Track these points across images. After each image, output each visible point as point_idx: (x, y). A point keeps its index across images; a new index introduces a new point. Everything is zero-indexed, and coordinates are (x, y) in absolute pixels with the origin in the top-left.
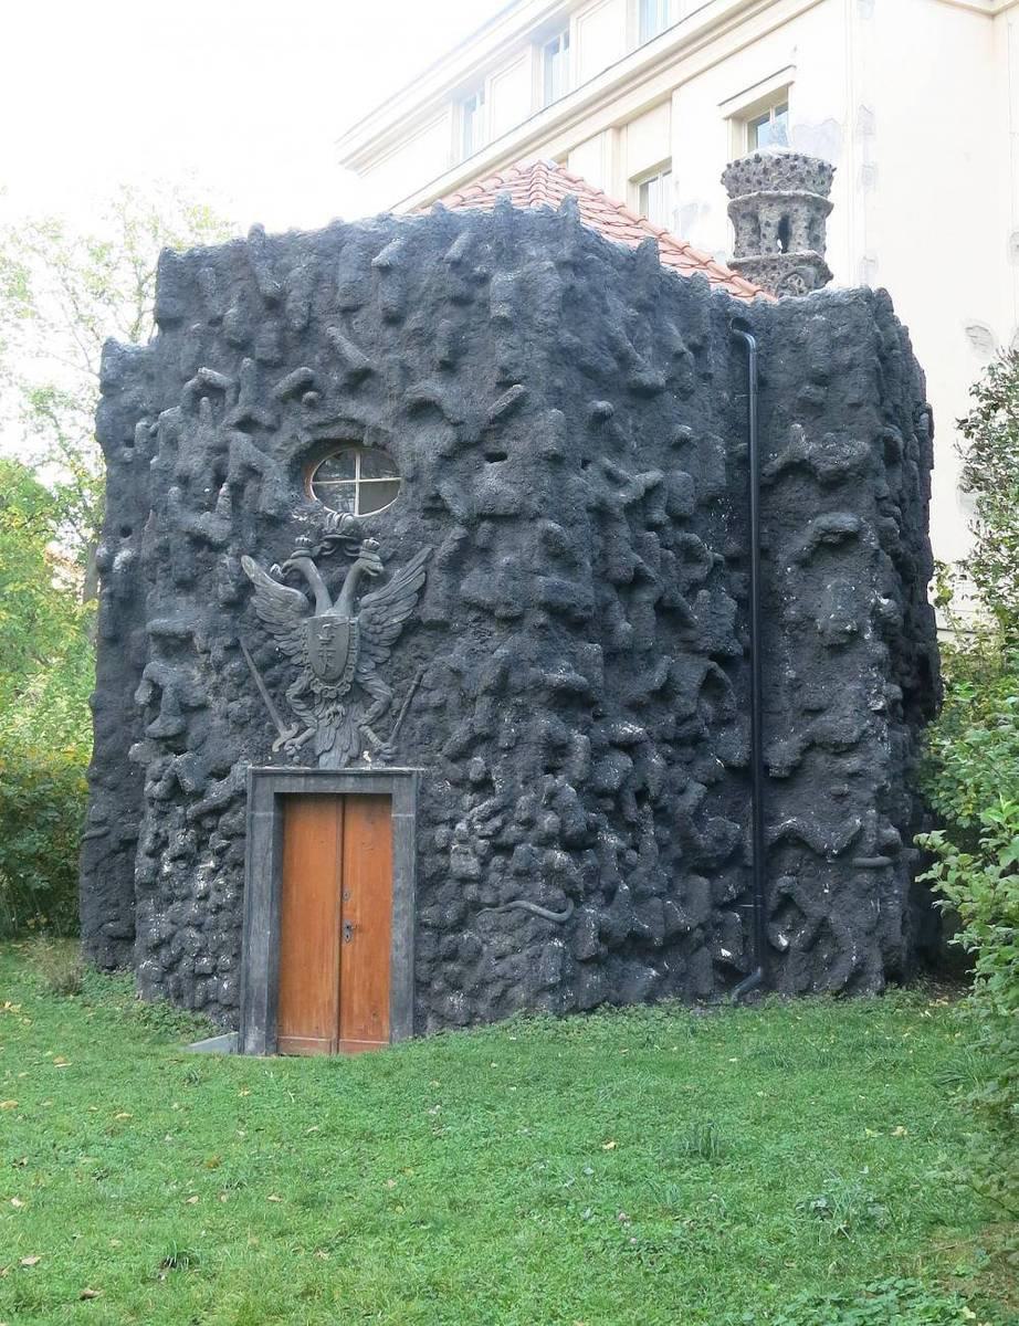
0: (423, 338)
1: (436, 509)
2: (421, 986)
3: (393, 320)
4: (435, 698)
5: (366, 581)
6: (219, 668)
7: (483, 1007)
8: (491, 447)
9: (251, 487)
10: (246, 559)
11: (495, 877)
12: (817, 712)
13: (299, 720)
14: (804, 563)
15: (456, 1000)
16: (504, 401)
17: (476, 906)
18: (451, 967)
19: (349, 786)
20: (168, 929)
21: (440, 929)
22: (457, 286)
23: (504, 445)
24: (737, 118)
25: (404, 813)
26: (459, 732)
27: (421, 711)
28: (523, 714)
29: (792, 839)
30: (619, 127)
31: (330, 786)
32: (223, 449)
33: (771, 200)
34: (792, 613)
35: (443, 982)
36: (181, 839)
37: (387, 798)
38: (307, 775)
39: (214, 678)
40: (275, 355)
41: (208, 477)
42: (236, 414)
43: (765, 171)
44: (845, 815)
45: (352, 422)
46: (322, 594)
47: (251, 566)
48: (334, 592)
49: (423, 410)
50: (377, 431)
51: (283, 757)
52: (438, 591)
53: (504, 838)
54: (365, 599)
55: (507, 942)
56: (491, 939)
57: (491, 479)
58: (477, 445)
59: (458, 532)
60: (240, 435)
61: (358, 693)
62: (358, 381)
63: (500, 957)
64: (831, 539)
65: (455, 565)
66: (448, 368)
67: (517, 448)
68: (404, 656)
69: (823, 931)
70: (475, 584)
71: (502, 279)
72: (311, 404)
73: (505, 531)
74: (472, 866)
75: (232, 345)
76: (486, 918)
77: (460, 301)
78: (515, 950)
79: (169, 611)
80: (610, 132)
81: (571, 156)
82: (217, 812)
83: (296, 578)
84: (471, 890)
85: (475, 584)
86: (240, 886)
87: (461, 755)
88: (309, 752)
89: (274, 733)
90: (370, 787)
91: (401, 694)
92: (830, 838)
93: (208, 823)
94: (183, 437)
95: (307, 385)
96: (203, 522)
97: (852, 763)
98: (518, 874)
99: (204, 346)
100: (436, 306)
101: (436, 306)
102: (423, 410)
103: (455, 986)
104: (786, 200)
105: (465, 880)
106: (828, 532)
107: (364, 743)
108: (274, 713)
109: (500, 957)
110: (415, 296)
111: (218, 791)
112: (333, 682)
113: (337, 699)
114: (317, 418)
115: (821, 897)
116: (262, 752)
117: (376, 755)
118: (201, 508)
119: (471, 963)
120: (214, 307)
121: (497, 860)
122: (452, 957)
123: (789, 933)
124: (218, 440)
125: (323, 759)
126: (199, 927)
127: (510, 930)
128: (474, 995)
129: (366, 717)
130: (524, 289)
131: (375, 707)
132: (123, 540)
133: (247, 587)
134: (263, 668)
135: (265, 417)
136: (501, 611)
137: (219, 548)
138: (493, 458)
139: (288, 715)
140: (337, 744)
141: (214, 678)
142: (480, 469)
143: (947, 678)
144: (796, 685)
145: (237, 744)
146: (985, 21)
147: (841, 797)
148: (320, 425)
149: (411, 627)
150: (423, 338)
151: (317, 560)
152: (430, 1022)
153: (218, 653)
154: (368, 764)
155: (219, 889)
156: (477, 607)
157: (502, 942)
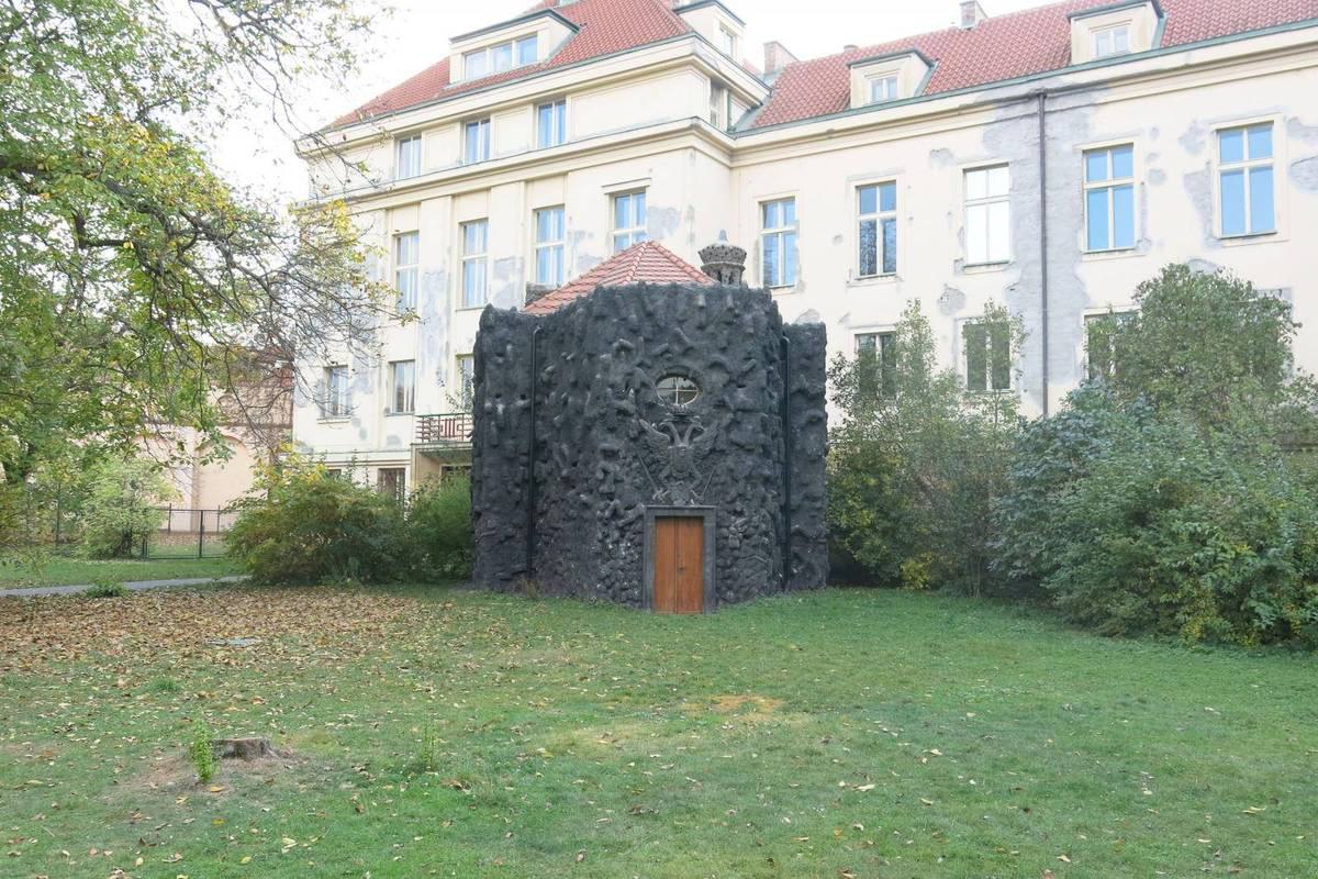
0: (713, 336)
1: (721, 405)
2: (718, 589)
3: (701, 327)
4: (723, 479)
5: (696, 432)
6: (630, 465)
7: (741, 596)
8: (740, 382)
9: (643, 390)
10: (641, 421)
11: (744, 547)
12: (806, 485)
13: (663, 486)
14: (802, 429)
15: (730, 594)
16: (746, 367)
17: (737, 558)
18: (729, 582)
19: (687, 513)
20: (609, 572)
21: (725, 567)
22: (729, 318)
23: (745, 382)
24: (611, 195)
25: (710, 524)
26: (733, 493)
27: (716, 485)
28: (754, 486)
29: (799, 533)
30: (403, 138)
31: (678, 513)
32: (631, 374)
33: (728, 266)
34: (798, 447)
35: (725, 589)
36: (616, 534)
37: (701, 519)
38: (669, 509)
39: (627, 469)
40: (651, 337)
41: (624, 386)
42: (638, 360)
43: (726, 253)
44: (815, 524)
45: (684, 367)
46: (677, 437)
47: (645, 424)
48: (682, 435)
49: (716, 365)
50: (695, 372)
51: (657, 501)
52: (723, 438)
53: (748, 532)
54: (695, 440)
55: (750, 571)
56: (744, 571)
57: (741, 395)
58: (736, 382)
59: (730, 416)
60: (638, 369)
61: (691, 477)
62: (687, 351)
63: (747, 577)
64: (814, 420)
65: (728, 429)
66: (723, 350)
67: (750, 383)
68: (708, 463)
69: (810, 567)
70: (735, 436)
71: (748, 317)
72: (669, 360)
73: (746, 415)
74: (737, 543)
75: (631, 330)
76: (741, 562)
77: (729, 324)
78: (752, 574)
79: (605, 440)
80: (523, 183)
81: (493, 190)
82: (631, 524)
83: (665, 429)
84: (736, 553)
85: (735, 436)
86: (641, 553)
87: (733, 501)
88: (669, 499)
89: (653, 492)
90: (696, 514)
91: (706, 477)
92: (811, 532)
93: (627, 528)
94: (612, 367)
95: (667, 351)
96: (624, 404)
97: (818, 505)
98: (754, 546)
99: (619, 328)
100: (718, 324)
101: (718, 324)
102: (716, 365)
103: (730, 588)
104: (733, 267)
105: (733, 549)
106: (814, 417)
107: (692, 496)
108: (653, 483)
109: (747, 577)
110: (711, 319)
111: (631, 514)
112: (681, 472)
113: (683, 479)
114: (671, 365)
115: (809, 555)
116: (647, 500)
117: (696, 501)
118: (622, 399)
119: (735, 580)
120: (623, 312)
121: (746, 541)
122: (729, 577)
123: (796, 568)
124: (630, 371)
125: (675, 503)
126: (622, 570)
127: (751, 567)
128: (736, 592)
129: (692, 486)
130: (755, 320)
131: (696, 482)
132: (498, 400)
133: (643, 432)
134: (649, 466)
135: (648, 362)
136: (748, 447)
137: (631, 415)
138: (740, 387)
139: (659, 484)
140: (681, 497)
141: (627, 469)
142: (735, 391)
143: (796, 470)
144: (798, 475)
145: (637, 496)
146: (726, 171)
147: (813, 517)
148: (670, 368)
149: (713, 451)
150: (713, 336)
151: (674, 422)
152: (721, 602)
153: (629, 459)
154: (693, 505)
155: (632, 555)
156: (737, 445)
157: (748, 572)
